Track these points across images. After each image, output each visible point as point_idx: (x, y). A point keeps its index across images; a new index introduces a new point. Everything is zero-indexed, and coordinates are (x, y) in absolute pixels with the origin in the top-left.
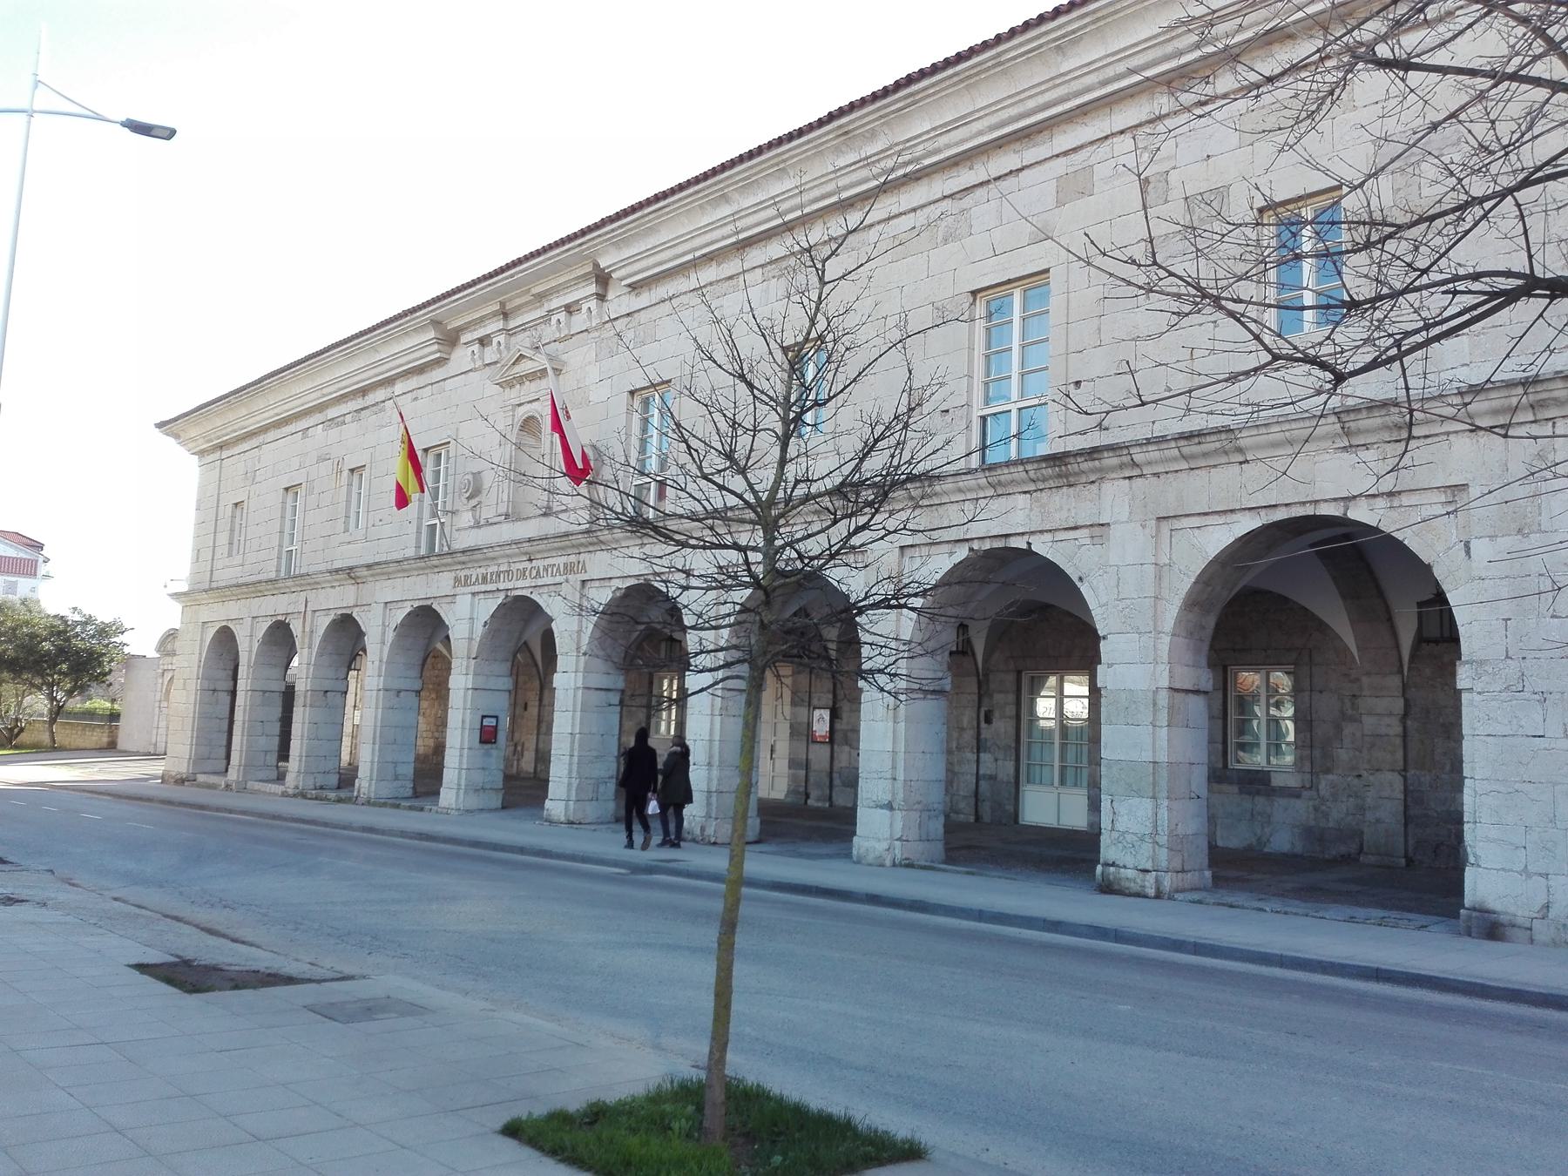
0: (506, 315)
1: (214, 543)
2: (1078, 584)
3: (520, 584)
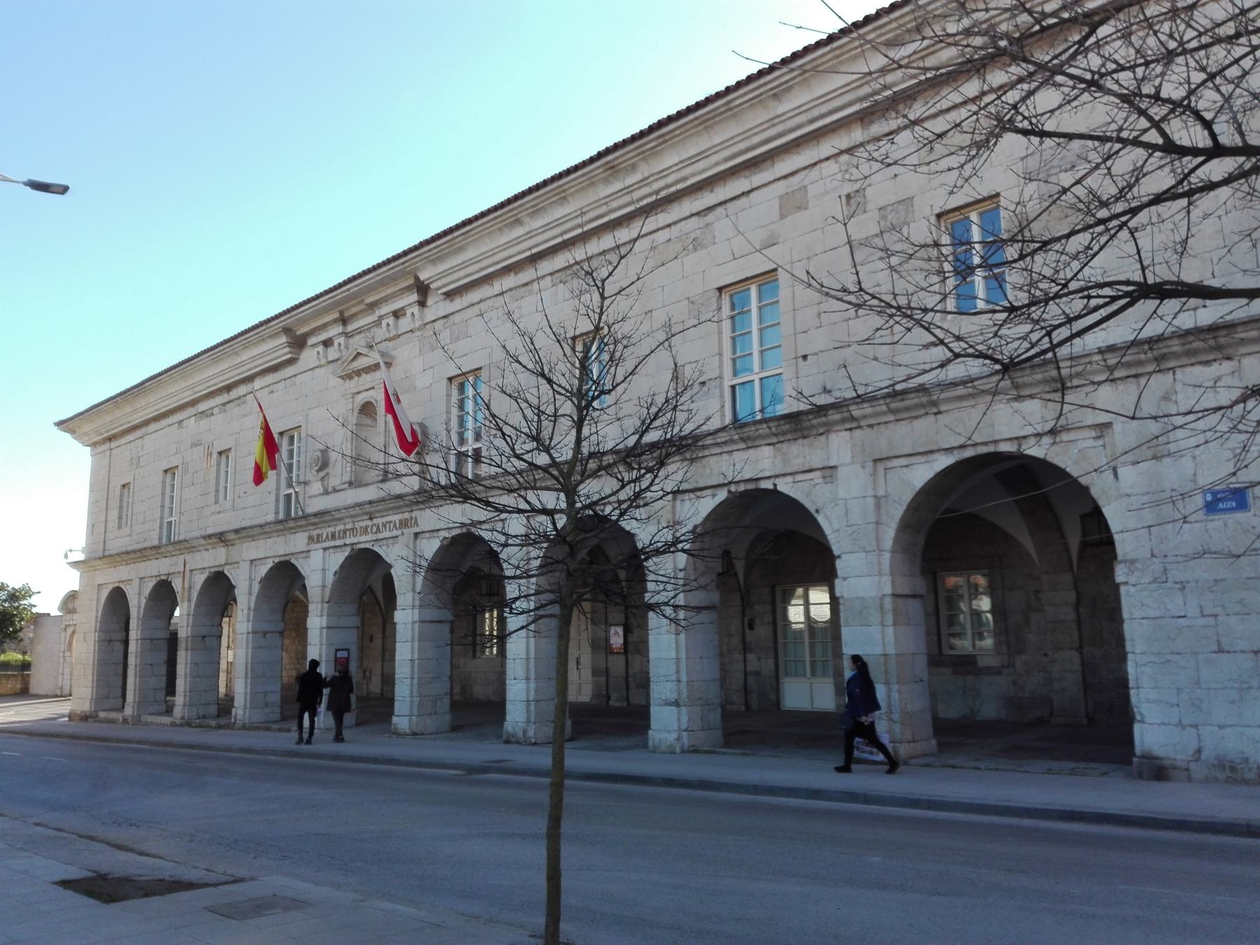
0: (344, 321)
3: (363, 538)
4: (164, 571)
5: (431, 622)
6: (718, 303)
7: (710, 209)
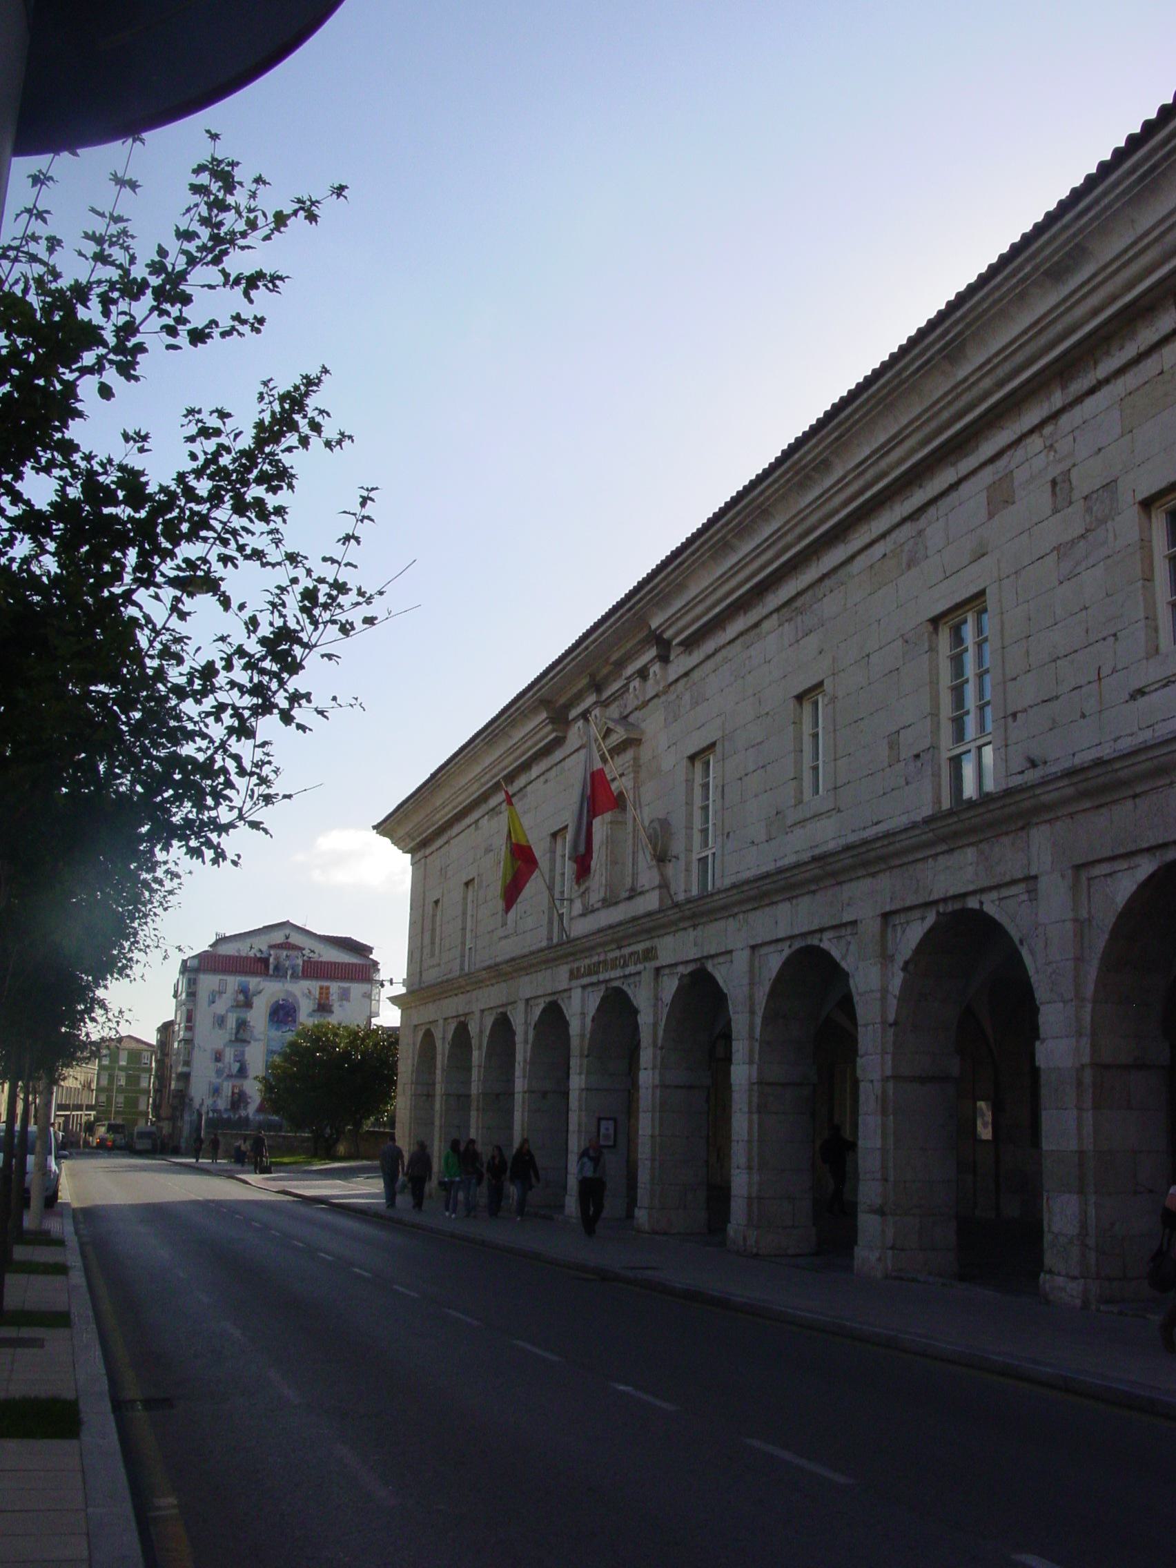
0: (598, 687)
1: (422, 944)
2: (1019, 947)
4: (693, 954)
5: (677, 1087)
6: (930, 641)
7: (922, 509)
